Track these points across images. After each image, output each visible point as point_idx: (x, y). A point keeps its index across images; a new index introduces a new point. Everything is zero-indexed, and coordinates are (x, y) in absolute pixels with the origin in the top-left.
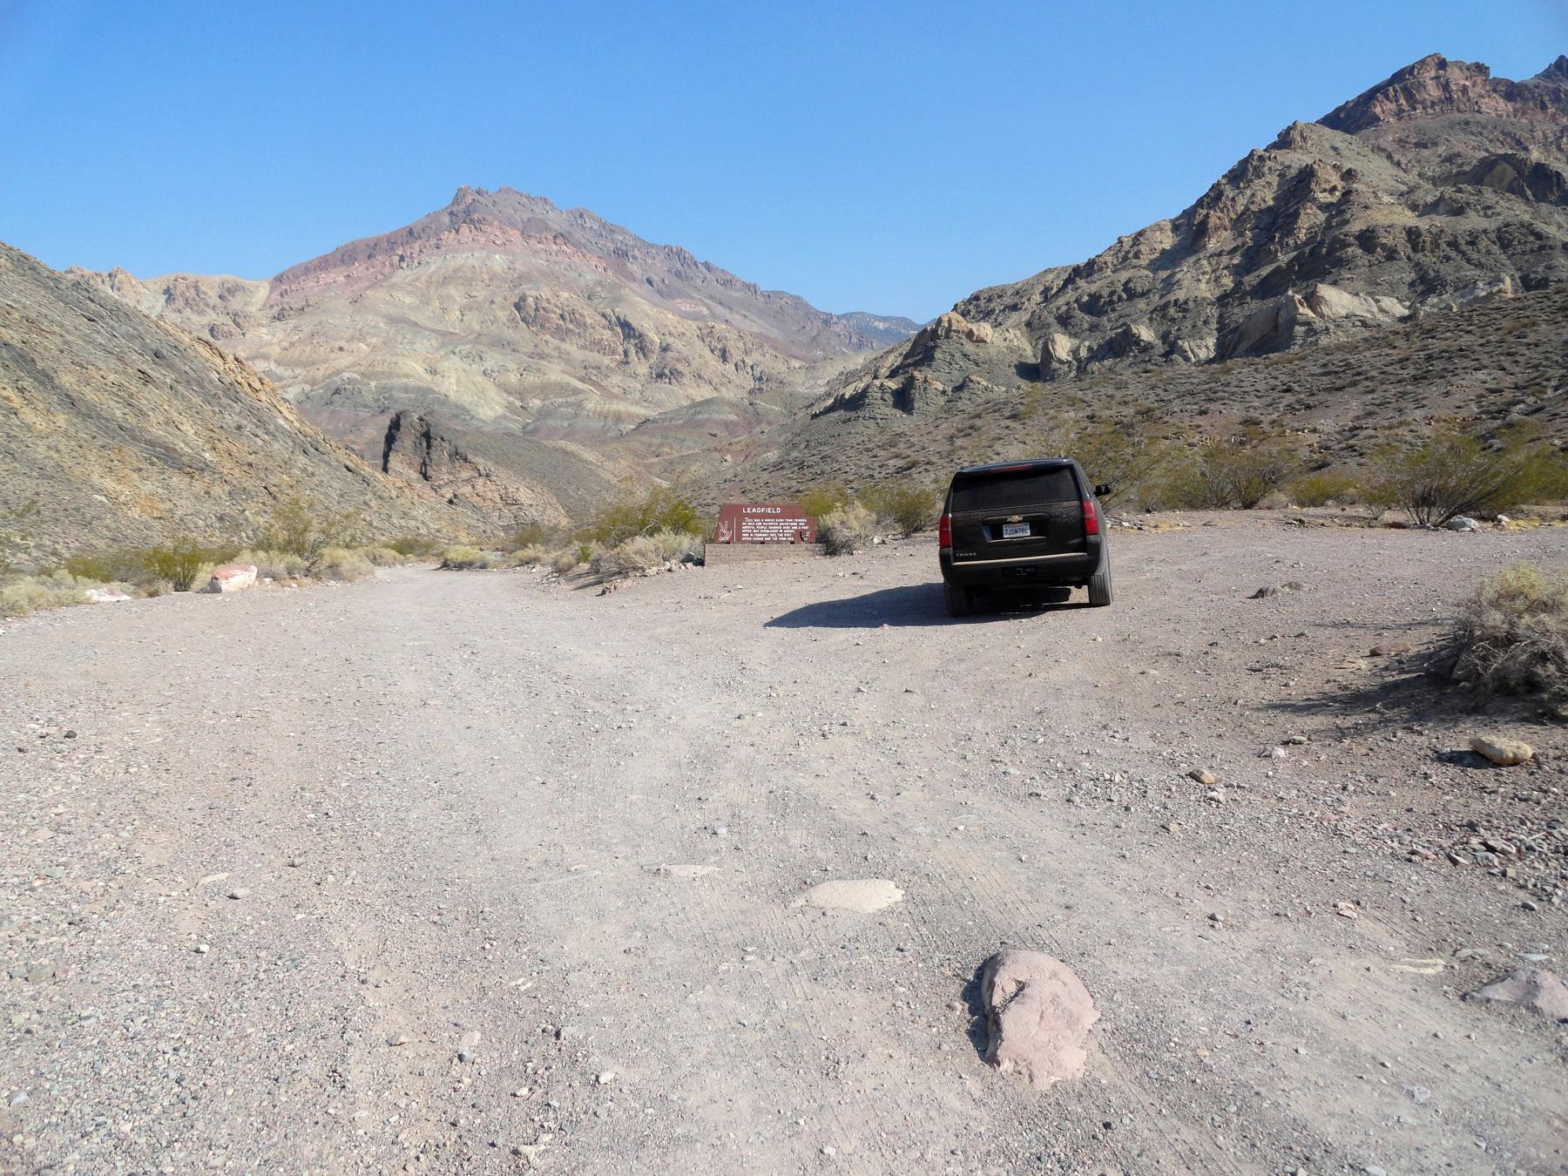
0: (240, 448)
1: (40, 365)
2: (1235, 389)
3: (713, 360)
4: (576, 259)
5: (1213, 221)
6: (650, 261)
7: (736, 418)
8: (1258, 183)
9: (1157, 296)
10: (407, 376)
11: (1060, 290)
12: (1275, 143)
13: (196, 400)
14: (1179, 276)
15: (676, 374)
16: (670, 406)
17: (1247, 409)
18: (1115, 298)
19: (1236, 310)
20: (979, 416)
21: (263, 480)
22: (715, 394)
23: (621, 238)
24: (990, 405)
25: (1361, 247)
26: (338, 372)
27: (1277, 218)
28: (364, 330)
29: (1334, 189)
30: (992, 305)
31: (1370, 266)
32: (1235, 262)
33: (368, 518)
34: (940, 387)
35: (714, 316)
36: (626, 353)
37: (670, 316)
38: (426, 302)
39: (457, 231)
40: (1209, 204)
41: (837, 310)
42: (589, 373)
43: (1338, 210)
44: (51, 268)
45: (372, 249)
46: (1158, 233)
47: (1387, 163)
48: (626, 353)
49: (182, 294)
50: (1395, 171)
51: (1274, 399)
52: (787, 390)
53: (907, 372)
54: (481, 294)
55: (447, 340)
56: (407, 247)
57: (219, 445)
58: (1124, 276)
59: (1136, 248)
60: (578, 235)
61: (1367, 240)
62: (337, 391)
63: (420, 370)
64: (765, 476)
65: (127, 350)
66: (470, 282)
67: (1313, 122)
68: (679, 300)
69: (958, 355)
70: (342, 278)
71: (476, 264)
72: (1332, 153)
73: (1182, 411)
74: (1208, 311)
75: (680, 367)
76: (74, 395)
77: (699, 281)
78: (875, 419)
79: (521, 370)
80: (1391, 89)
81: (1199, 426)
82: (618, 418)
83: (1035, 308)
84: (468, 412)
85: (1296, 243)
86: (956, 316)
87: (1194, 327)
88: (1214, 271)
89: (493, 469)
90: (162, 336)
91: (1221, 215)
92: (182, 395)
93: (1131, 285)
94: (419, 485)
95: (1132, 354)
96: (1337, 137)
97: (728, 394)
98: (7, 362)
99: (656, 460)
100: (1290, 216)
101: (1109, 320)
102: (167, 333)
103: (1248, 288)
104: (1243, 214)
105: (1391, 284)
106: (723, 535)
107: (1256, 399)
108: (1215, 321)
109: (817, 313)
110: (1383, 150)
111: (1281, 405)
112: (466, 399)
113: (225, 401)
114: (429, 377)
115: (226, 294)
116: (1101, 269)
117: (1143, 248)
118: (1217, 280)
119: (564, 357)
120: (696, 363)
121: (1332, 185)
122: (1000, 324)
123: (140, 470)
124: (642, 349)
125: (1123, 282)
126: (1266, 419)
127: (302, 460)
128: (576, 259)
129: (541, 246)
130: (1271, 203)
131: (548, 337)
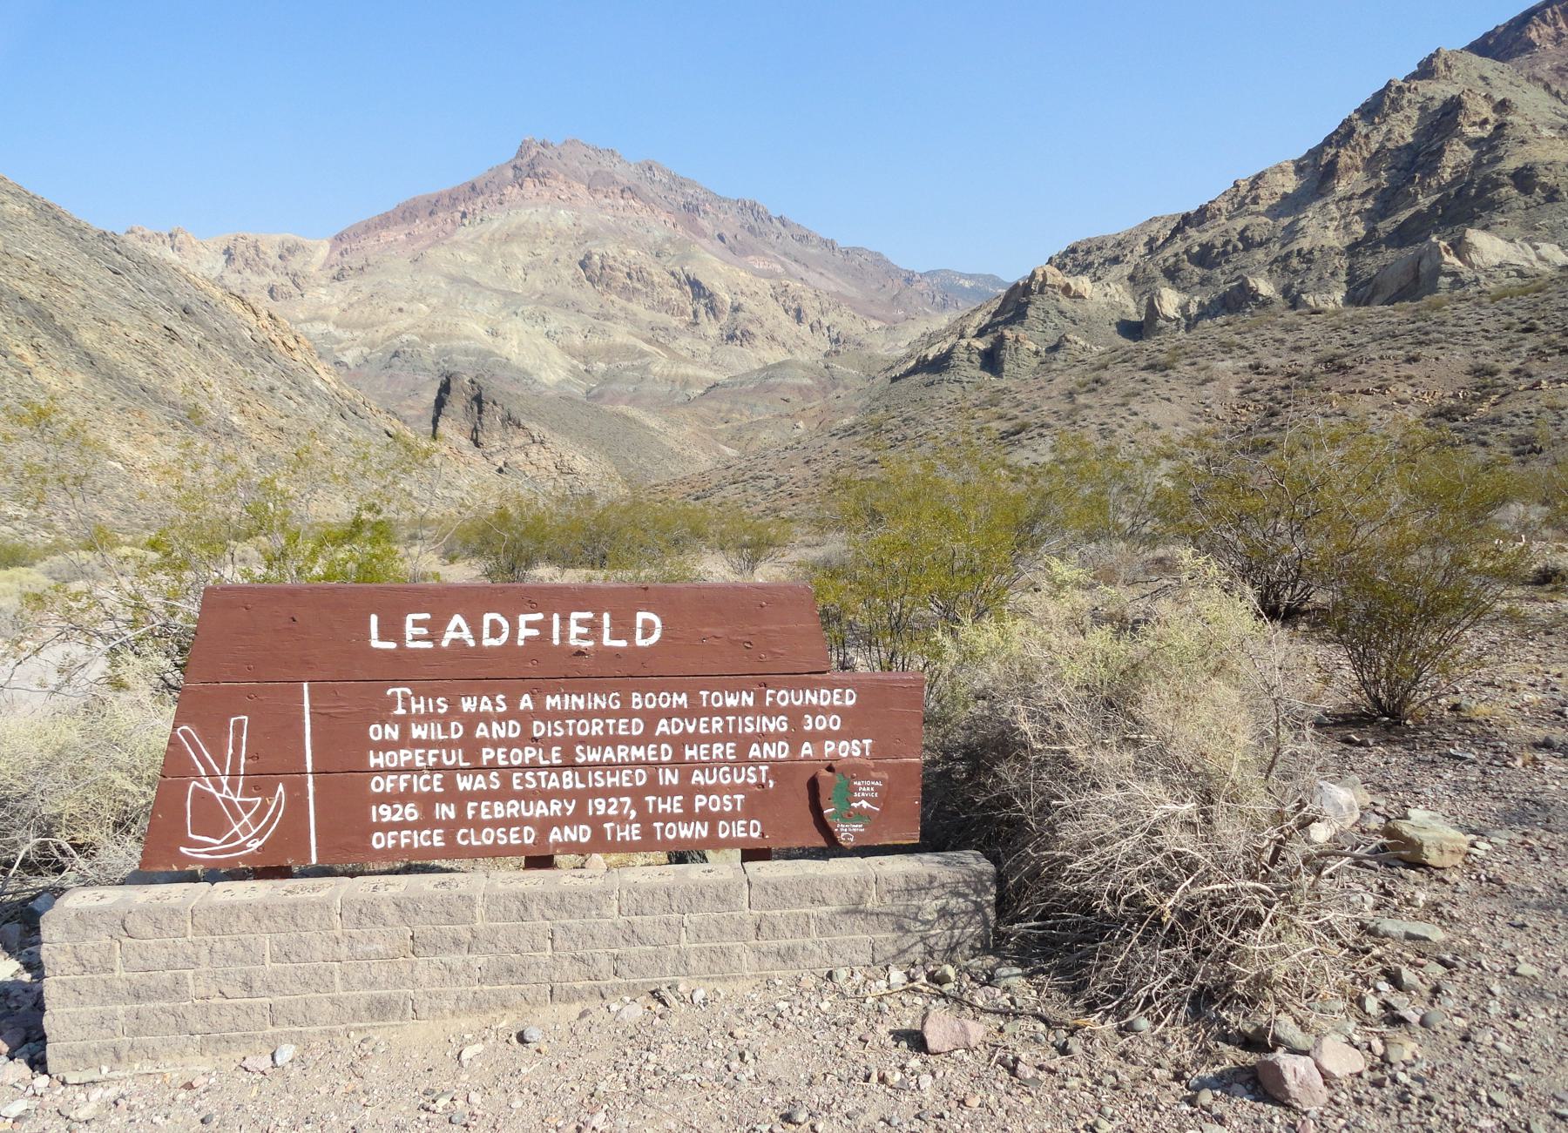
0: (271, 414)
1: (59, 321)
2: (1454, 329)
3: (787, 321)
4: (644, 214)
5: (1343, 160)
6: (722, 216)
7: (810, 382)
8: (1395, 118)
9: (1278, 246)
10: (467, 338)
11: (1167, 240)
12: (1414, 73)
13: (226, 359)
14: (1303, 223)
15: (747, 335)
16: (741, 368)
17: (1475, 355)
18: (1230, 248)
19: (1369, 260)
20: (1105, 367)
21: (295, 446)
22: (789, 357)
23: (691, 192)
24: (1119, 353)
25: (1516, 186)
26: (398, 334)
27: (1417, 156)
28: (425, 290)
29: (1485, 121)
30: (1091, 258)
31: (1527, 208)
32: (1368, 206)
33: (408, 488)
34: (1033, 347)
35: (789, 275)
36: (695, 313)
37: (742, 274)
38: (488, 260)
39: (521, 186)
40: (1338, 142)
41: (920, 268)
42: (657, 334)
43: (1489, 146)
44: (76, 217)
45: (433, 207)
46: (1279, 175)
47: (1544, 94)
48: (695, 313)
49: (242, 255)
50: (1554, 102)
51: (1511, 341)
52: (866, 352)
53: (997, 331)
54: (545, 252)
55: (510, 300)
56: (470, 203)
57: (248, 408)
58: (1240, 224)
59: (1254, 193)
60: (646, 188)
61: (1524, 179)
62: (396, 354)
63: (481, 331)
64: (834, 442)
65: (152, 305)
66: (534, 238)
67: (1459, 49)
68: (752, 257)
69: (1053, 312)
70: (403, 237)
71: (540, 221)
72: (1480, 83)
73: (1381, 358)
74: (1336, 261)
75: (752, 328)
76: (94, 353)
77: (773, 237)
78: (960, 382)
79: (586, 332)
80: (1549, 10)
81: (1409, 377)
82: (686, 382)
83: (1138, 260)
84: (530, 376)
85: (1439, 184)
86: (1051, 269)
87: (1320, 279)
88: (1343, 217)
89: (547, 436)
90: (192, 290)
91: (1351, 153)
92: (212, 355)
93: (1249, 233)
94: (469, 452)
95: (1248, 310)
96: (1487, 66)
97: (803, 357)
98: (22, 318)
99: (724, 426)
100: (1432, 154)
101: (1223, 273)
102: (197, 287)
103: (1383, 235)
104: (1377, 152)
105: (1552, 229)
106: (212, 819)
107: (1486, 342)
108: (1344, 272)
109: (898, 270)
110: (1540, 80)
111: (1523, 349)
112: (528, 363)
113: (258, 360)
114: (490, 339)
115: (286, 254)
116: (1214, 217)
117: (1262, 192)
118: (1347, 226)
119: (631, 318)
120: (768, 324)
121: (1483, 117)
122: (1099, 279)
123: (162, 434)
124: (712, 309)
125: (1239, 230)
126: (1505, 368)
127: (339, 425)
128: (644, 214)
129: (608, 201)
130: (1410, 140)
131: (614, 297)
